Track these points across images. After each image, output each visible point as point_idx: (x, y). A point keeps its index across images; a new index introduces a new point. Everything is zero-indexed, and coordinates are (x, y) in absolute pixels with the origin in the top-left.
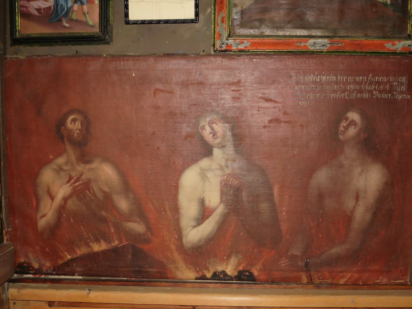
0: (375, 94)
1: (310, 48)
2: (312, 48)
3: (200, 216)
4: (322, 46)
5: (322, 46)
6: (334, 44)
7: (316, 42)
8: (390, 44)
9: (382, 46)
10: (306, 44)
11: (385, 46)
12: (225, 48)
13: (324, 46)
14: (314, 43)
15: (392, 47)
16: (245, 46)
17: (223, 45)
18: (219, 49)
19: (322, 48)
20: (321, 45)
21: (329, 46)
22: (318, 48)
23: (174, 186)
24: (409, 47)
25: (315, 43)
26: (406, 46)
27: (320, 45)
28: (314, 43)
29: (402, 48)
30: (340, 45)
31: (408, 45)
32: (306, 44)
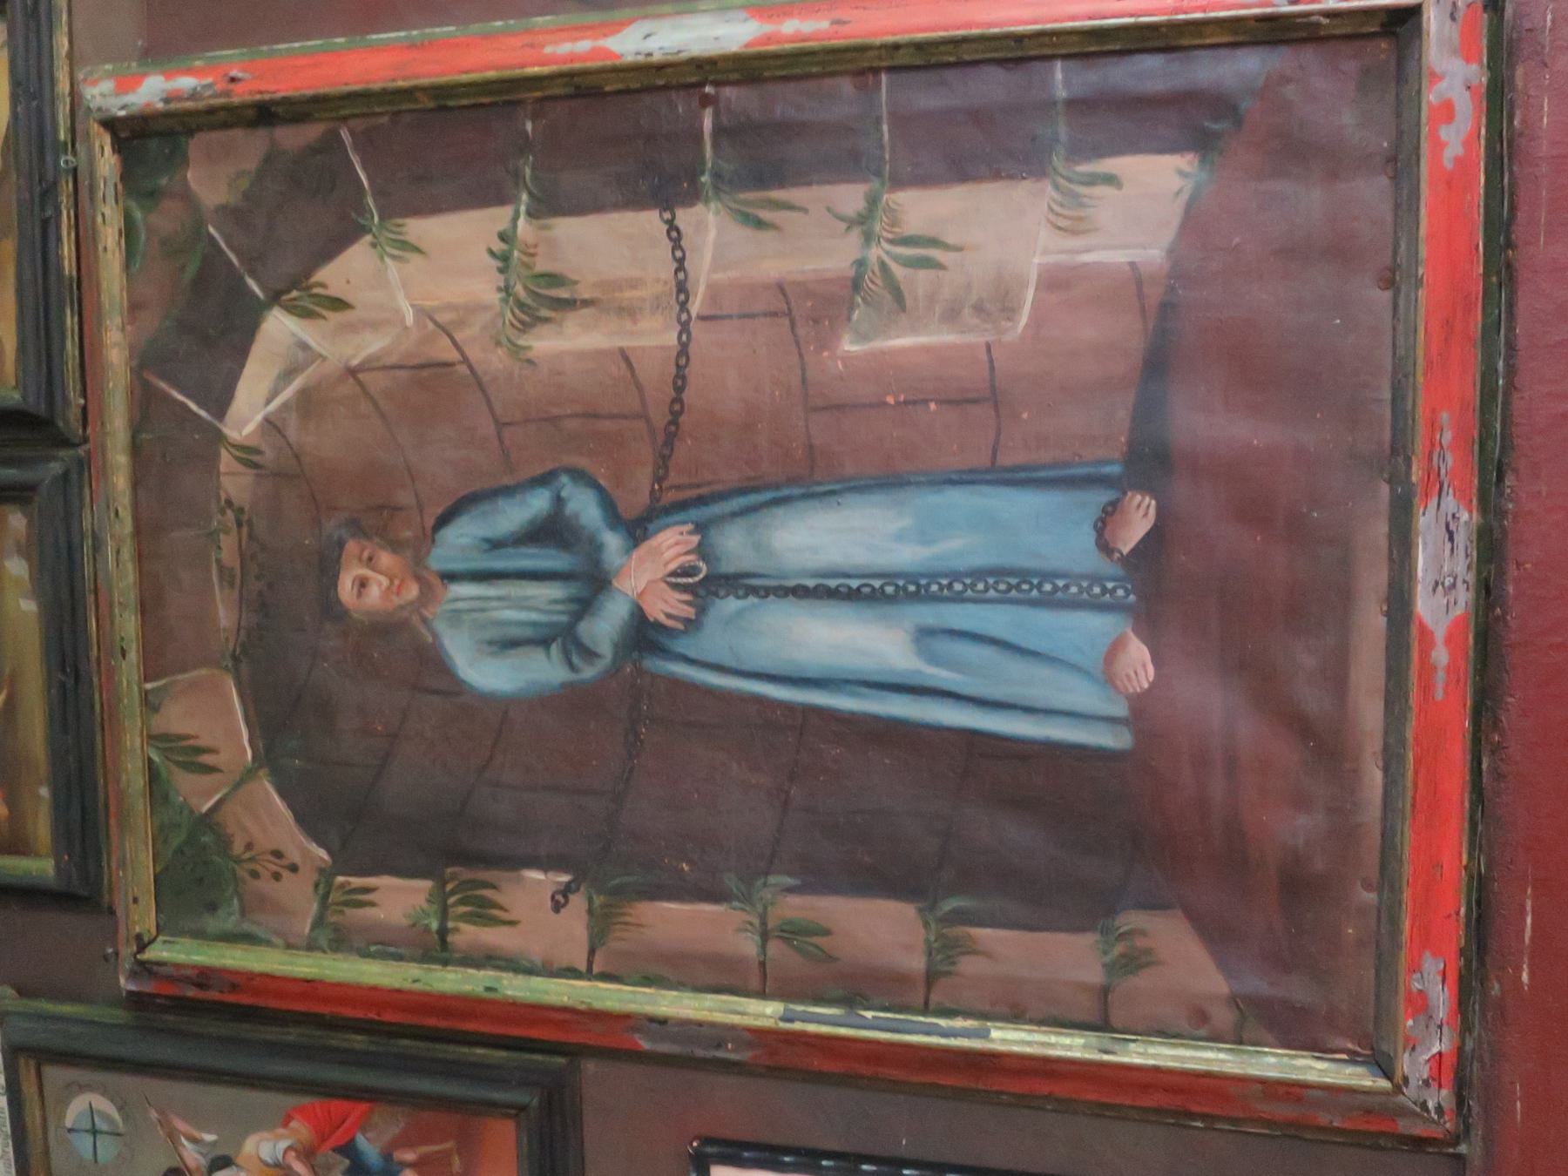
0: (467, 934)
1: (1459, 611)
2: (1464, 598)
3: (218, 824)
4: (1451, 539)
5: (1451, 539)
6: (1443, 471)
7: (1431, 579)
8: (1445, 133)
9: (1453, 182)
10: (1440, 634)
11: (1458, 161)
12: (1444, 1092)
13: (1452, 527)
14: (1434, 590)
15: (1459, 116)
16: (1439, 978)
17: (1431, 1105)
18: (1448, 1125)
19: (1461, 538)
20: (1448, 546)
21: (1451, 497)
22: (1461, 565)
23: (926, 1003)
24: (1460, 15)
25: (1437, 583)
26: (1453, 32)
27: (1447, 552)
28: (1434, 590)
29: (1468, 60)
30: (1447, 437)
31: (1449, 22)
32: (1440, 634)
